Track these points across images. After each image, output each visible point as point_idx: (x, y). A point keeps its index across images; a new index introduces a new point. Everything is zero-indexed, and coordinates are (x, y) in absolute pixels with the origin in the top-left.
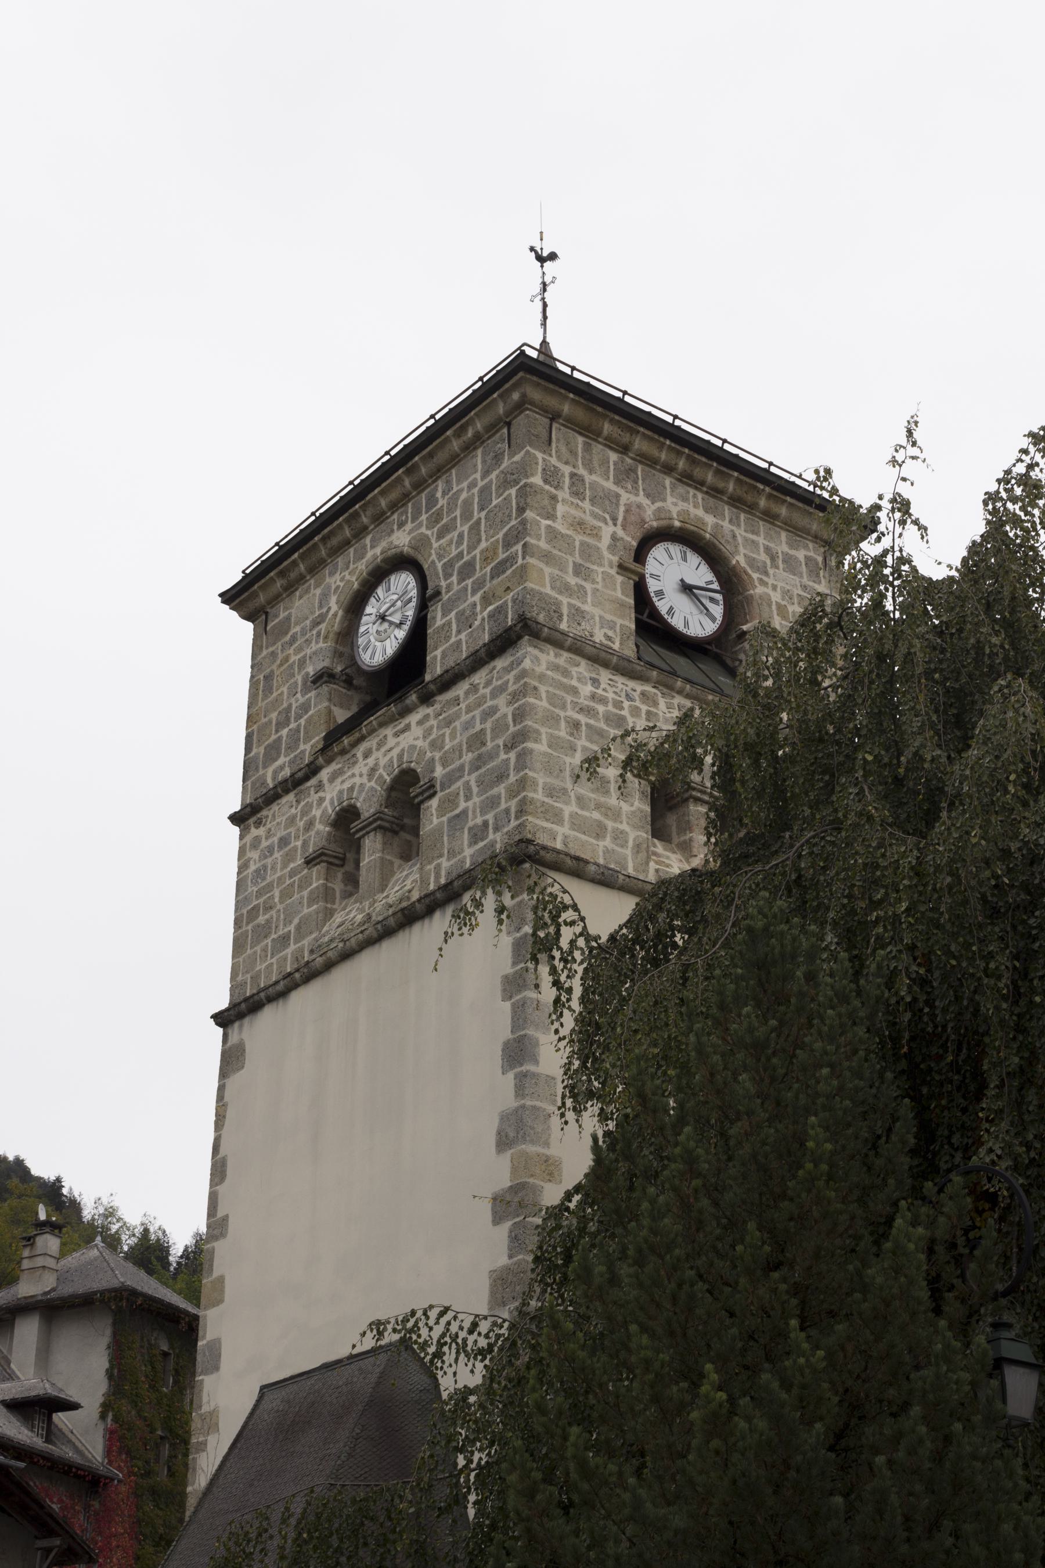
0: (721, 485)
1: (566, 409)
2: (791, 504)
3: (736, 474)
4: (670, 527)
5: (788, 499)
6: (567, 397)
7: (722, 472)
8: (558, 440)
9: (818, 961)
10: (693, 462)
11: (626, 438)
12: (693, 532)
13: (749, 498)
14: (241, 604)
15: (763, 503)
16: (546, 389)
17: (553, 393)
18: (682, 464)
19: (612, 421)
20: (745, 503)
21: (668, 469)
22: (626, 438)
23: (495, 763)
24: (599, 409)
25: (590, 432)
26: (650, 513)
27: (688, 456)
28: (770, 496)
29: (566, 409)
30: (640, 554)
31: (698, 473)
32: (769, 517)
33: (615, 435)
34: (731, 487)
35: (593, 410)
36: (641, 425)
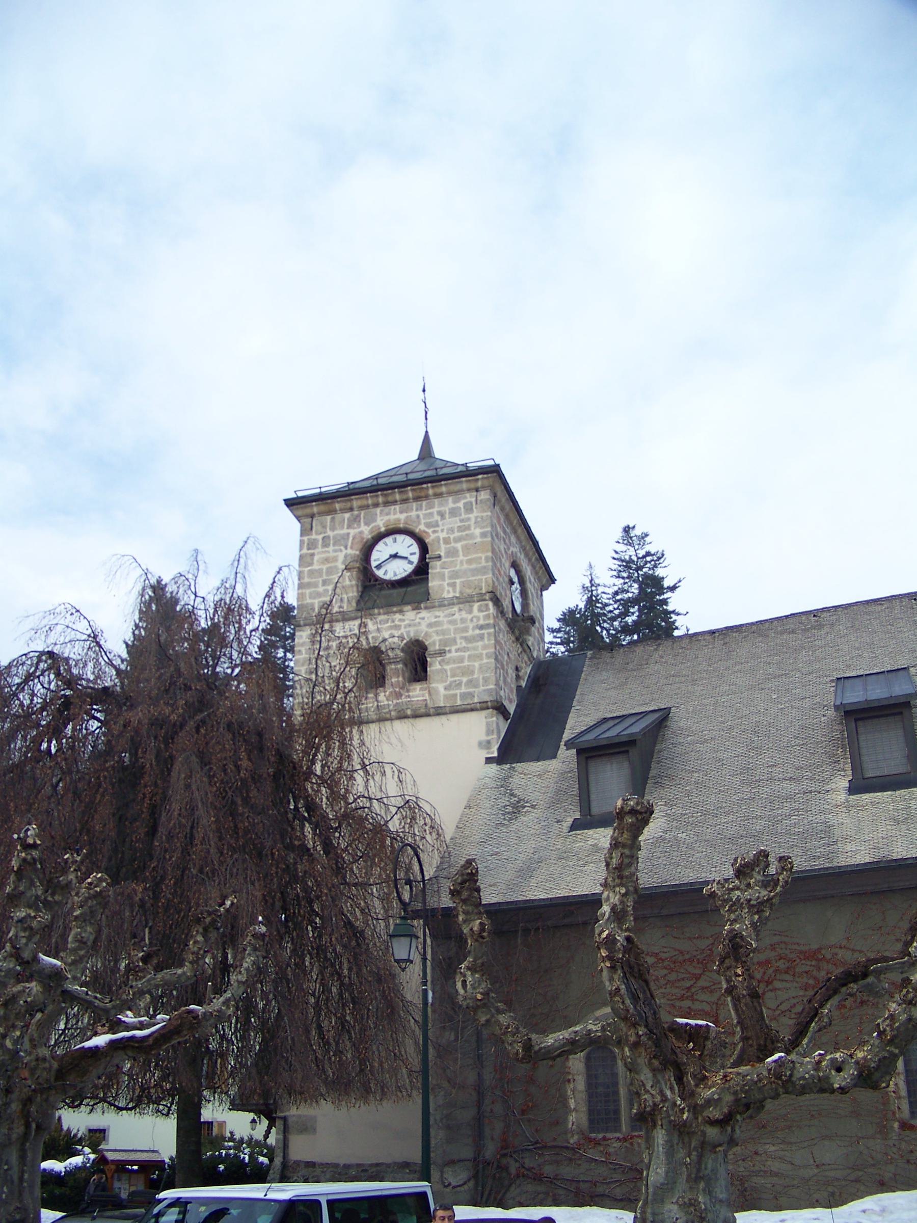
0: (405, 497)
1: (315, 510)
2: (445, 484)
3: (409, 488)
4: (380, 533)
5: (443, 483)
6: (352, 500)
7: (402, 492)
8: (316, 525)
9: (88, 979)
10: (386, 495)
11: (349, 505)
12: (393, 528)
13: (423, 494)
14: (486, 1202)
15: (431, 492)
16: (302, 508)
17: (305, 507)
18: (381, 500)
19: (338, 502)
20: (422, 497)
21: (376, 505)
22: (349, 505)
23: (622, 1099)
24: (329, 501)
25: (332, 512)
26: (366, 531)
27: (382, 495)
28: (433, 487)
29: (315, 510)
30: (424, 548)
31: (390, 498)
32: (438, 495)
33: (342, 507)
34: (410, 495)
35: (327, 503)
36: (478, 474)
